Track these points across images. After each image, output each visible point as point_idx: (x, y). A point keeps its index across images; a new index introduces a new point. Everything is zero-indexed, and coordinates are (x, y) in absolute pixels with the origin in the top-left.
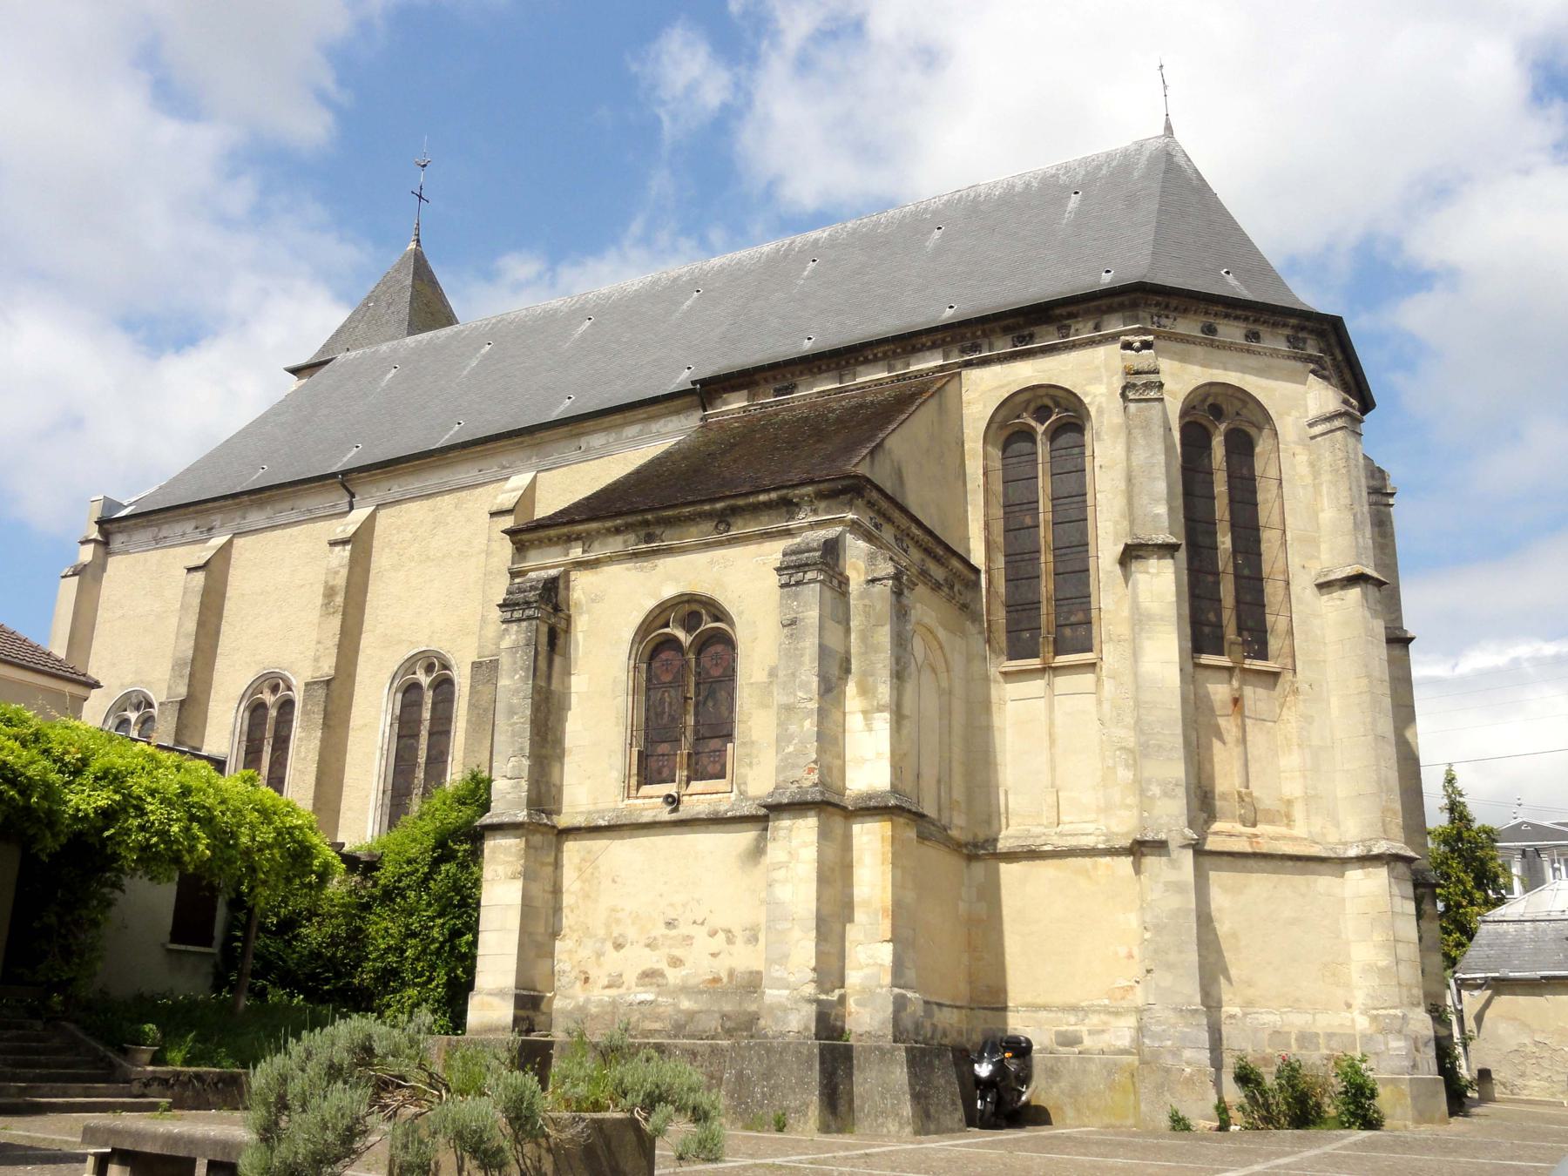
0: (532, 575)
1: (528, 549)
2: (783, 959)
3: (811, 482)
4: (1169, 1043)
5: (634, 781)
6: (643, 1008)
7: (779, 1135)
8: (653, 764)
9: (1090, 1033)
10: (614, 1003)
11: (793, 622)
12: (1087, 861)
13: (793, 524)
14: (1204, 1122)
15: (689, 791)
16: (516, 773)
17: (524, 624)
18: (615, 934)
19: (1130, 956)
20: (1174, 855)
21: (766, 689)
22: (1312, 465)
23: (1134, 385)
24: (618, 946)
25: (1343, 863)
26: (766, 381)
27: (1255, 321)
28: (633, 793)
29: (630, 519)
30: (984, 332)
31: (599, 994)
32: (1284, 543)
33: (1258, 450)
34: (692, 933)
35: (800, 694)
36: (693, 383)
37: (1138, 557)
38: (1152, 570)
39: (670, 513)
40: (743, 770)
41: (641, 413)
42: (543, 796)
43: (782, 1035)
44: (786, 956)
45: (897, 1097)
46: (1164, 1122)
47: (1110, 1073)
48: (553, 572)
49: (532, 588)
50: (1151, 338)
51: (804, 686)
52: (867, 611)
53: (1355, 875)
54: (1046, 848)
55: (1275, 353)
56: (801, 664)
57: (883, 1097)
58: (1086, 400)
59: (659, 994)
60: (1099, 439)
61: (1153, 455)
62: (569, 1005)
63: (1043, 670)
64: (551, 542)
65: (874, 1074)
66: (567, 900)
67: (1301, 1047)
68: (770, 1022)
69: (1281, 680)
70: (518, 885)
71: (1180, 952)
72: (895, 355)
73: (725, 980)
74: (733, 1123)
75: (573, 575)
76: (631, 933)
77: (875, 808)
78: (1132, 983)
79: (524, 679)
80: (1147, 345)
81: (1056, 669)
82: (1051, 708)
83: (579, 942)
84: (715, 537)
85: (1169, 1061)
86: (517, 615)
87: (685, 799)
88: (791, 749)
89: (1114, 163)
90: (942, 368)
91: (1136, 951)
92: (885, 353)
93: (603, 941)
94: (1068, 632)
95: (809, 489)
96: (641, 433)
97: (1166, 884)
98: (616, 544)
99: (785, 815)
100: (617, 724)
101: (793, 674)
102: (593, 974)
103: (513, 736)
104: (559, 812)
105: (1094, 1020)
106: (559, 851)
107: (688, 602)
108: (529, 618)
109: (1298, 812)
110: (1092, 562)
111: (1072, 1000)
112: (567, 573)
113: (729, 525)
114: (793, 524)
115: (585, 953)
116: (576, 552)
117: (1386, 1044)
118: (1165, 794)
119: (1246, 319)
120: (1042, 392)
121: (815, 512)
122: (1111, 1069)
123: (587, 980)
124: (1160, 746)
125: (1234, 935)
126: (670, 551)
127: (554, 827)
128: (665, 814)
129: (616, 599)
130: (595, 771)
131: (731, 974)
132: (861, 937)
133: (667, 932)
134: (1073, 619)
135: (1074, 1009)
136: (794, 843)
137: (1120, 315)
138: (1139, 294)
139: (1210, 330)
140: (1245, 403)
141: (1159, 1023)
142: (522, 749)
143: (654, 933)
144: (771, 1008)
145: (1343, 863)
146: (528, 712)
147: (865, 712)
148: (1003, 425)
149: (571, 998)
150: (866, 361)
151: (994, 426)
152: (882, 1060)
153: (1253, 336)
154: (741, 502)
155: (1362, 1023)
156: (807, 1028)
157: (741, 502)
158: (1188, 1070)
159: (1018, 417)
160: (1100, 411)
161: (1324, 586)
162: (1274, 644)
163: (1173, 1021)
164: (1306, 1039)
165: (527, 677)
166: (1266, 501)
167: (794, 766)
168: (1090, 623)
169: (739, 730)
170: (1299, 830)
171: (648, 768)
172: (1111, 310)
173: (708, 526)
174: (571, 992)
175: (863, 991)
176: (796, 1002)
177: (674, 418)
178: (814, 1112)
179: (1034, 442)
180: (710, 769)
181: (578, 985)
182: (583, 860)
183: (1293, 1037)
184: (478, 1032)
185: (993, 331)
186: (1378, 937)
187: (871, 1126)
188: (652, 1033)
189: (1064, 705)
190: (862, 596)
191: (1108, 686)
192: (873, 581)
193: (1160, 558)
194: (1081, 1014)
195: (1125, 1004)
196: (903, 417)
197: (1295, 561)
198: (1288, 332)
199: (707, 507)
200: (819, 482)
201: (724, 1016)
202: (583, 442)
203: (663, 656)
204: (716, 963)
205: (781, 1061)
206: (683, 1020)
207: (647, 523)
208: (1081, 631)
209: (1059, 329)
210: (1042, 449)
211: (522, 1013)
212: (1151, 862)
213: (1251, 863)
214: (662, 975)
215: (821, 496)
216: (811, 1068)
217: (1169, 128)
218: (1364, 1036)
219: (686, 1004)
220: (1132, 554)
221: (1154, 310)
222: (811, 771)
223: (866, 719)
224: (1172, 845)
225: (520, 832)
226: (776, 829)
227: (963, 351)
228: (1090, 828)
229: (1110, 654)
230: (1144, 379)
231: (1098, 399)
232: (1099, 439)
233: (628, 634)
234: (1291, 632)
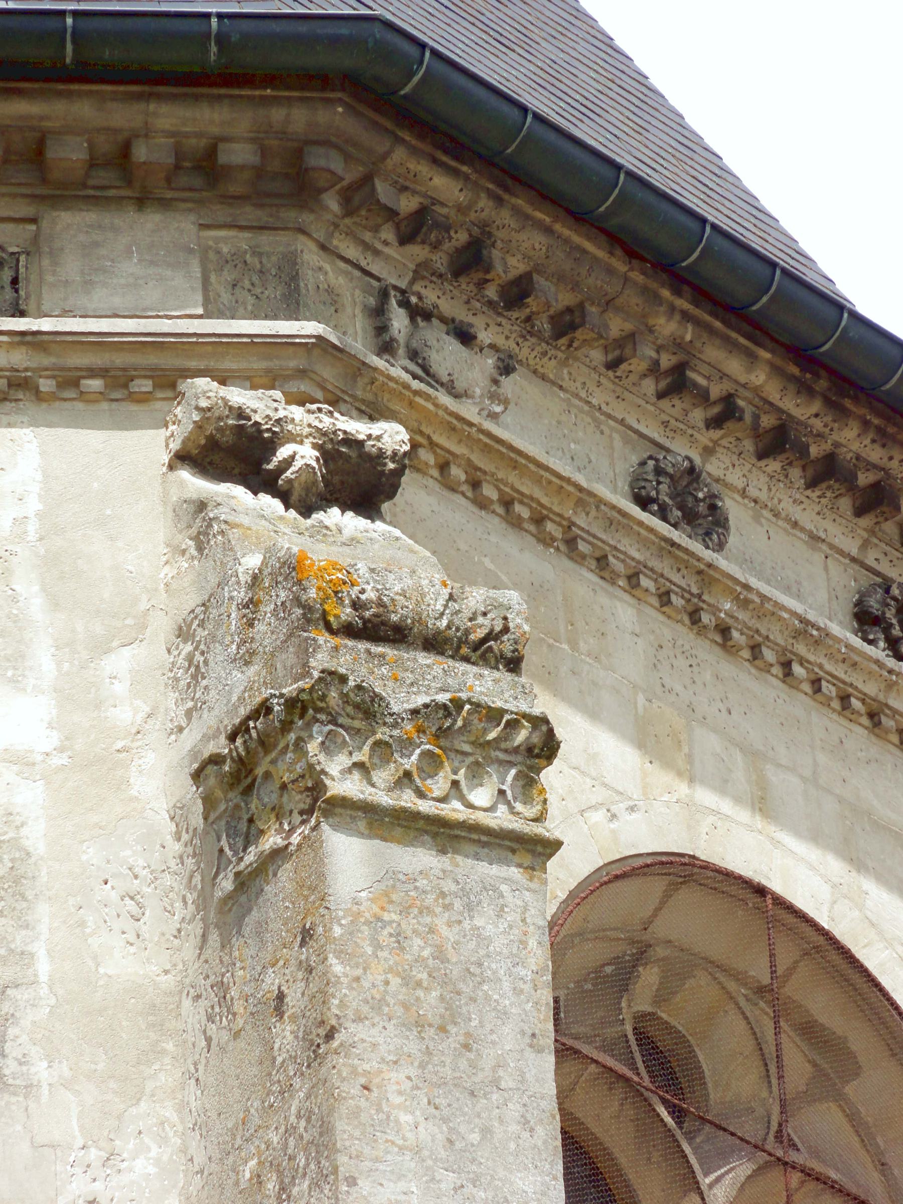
23: (368, 708)
80: (359, 483)
137: (181, 227)
138: (335, 116)
196: (389, 124)
221: (394, 263)
230: (411, 683)
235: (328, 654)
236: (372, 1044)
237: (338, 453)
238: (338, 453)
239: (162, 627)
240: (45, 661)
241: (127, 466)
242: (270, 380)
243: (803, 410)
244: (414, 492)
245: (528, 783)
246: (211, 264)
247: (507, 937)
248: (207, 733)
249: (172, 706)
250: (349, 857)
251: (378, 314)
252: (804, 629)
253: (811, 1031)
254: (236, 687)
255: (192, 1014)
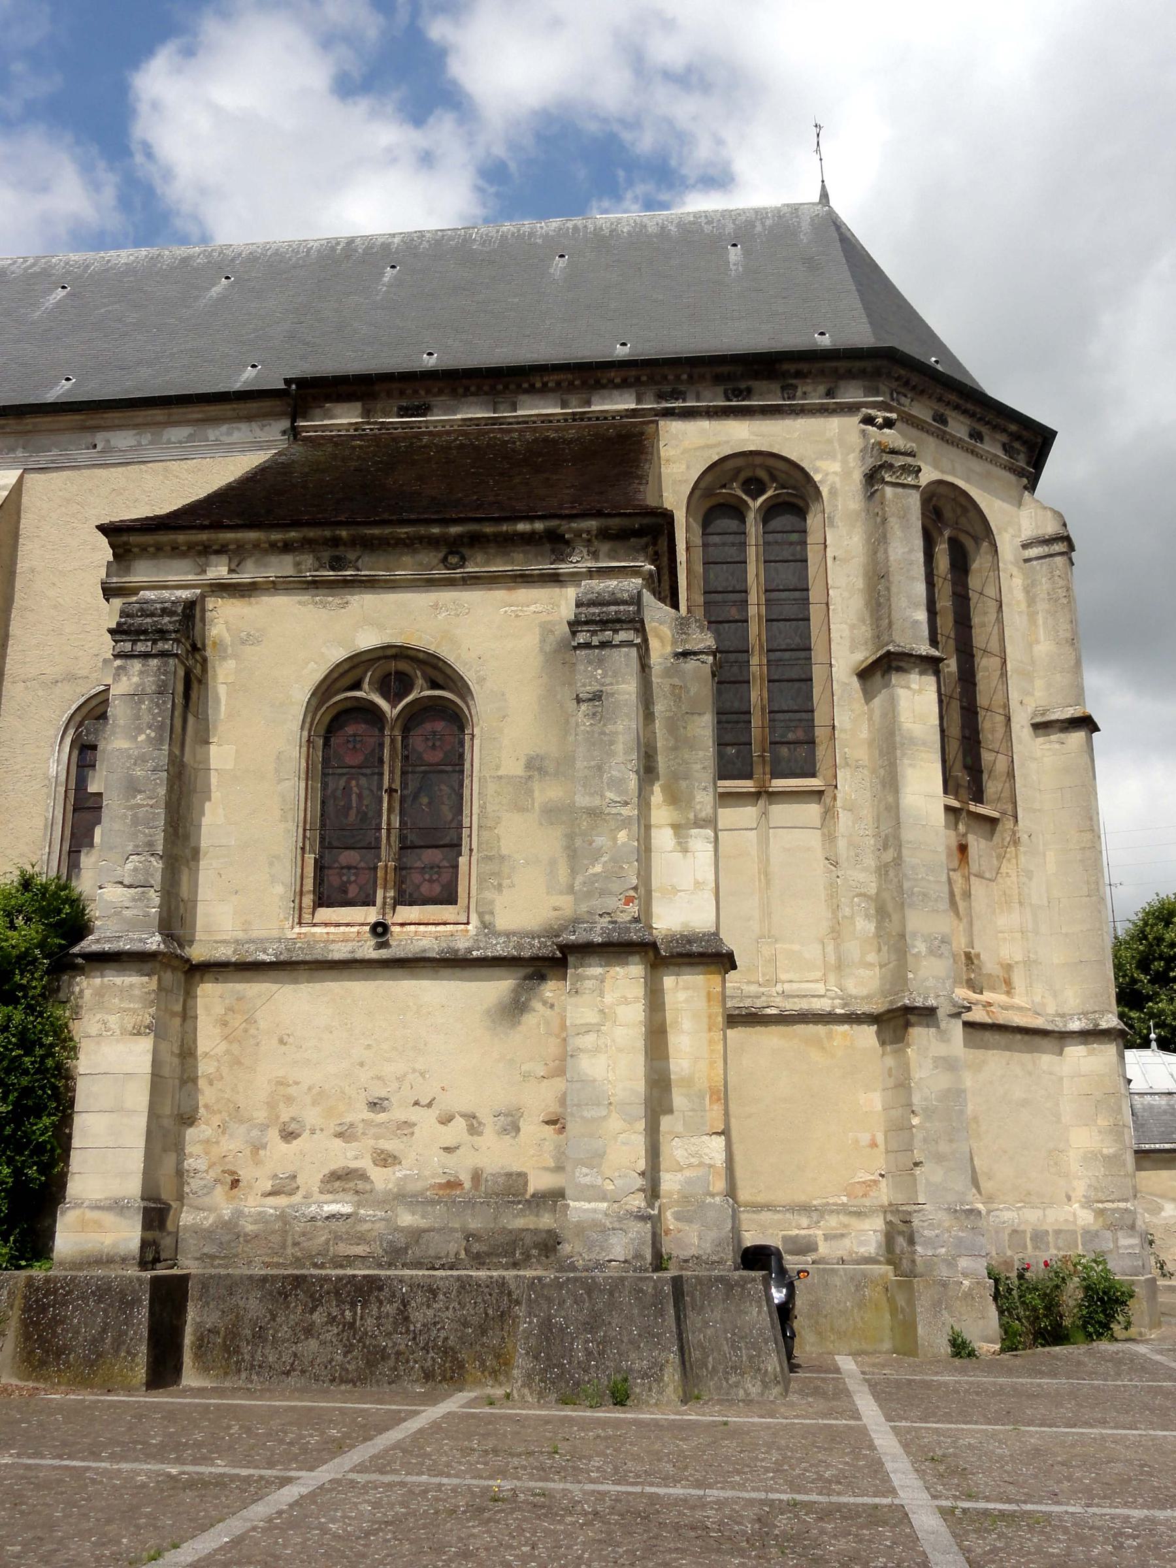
0: (150, 595)
1: (137, 557)
2: (595, 1159)
3: (599, 514)
4: (943, 1250)
5: (308, 900)
6: (334, 1225)
7: (618, 1414)
8: (333, 878)
9: (827, 1237)
10: (283, 1217)
11: (597, 697)
12: (820, 1029)
13: (564, 568)
14: (987, 1347)
15: (398, 918)
16: (141, 878)
17: (154, 662)
18: (285, 1117)
19: (874, 1145)
20: (943, 1025)
21: (523, 786)
22: (1027, 590)
23: (891, 466)
24: (289, 1135)
25: (1063, 1037)
26: (389, 395)
27: (980, 420)
28: (307, 917)
29: (312, 533)
30: (691, 377)
31: (256, 1205)
32: (1004, 674)
33: (975, 566)
34: (413, 1119)
35: (610, 795)
36: (288, 382)
37: (899, 669)
38: (915, 686)
39: (376, 531)
40: (488, 895)
41: (195, 412)
42: (175, 919)
43: (599, 1266)
44: (600, 1155)
45: (754, 1346)
46: (946, 1349)
47: (858, 1287)
48: (185, 594)
49: (165, 612)
50: (894, 416)
51: (617, 784)
52: (677, 693)
53: (1075, 1052)
54: (769, 1011)
55: (993, 460)
56: (611, 754)
57: (734, 1347)
58: (817, 478)
59: (359, 1205)
60: (832, 525)
61: (911, 551)
62: (207, 1220)
63: (757, 795)
64: (176, 552)
65: (717, 1315)
66: (205, 1067)
67: (1036, 1248)
68: (578, 1248)
69: (1000, 827)
70: (144, 1047)
71: (951, 1141)
72: (571, 388)
73: (467, 1185)
74: (541, 1395)
75: (210, 603)
76: (312, 1116)
77: (701, 955)
78: (876, 1177)
79: (157, 742)
80: (888, 424)
81: (773, 793)
82: (764, 842)
83: (223, 1128)
84: (440, 572)
85: (944, 1272)
86: (141, 647)
87: (395, 929)
88: (598, 868)
89: (768, 222)
90: (634, 413)
91: (880, 1139)
92: (558, 384)
93: (264, 1128)
94: (784, 751)
95: (592, 524)
96: (191, 438)
97: (936, 1059)
98: (282, 567)
99: (594, 960)
100: (284, 819)
101: (599, 768)
102: (244, 1174)
103: (135, 821)
104: (191, 942)
105: (832, 1221)
106: (189, 995)
107: (395, 657)
108: (163, 654)
109: (1018, 979)
110: (817, 672)
111: (801, 1198)
112: (203, 597)
113: (463, 559)
114: (564, 568)
115: (232, 1144)
116: (219, 571)
117: (1116, 1241)
118: (931, 952)
119: (972, 415)
120: (758, 460)
121: (595, 555)
122: (859, 1283)
123: (235, 1183)
124: (925, 895)
125: (975, 1119)
126: (371, 584)
127: (188, 961)
128: (368, 950)
129: (281, 646)
130: (249, 882)
131: (476, 1176)
132: (679, 1128)
133: (371, 1116)
134: (791, 736)
135: (805, 1209)
136: (608, 999)
137: (860, 383)
139: (941, 419)
140: (965, 510)
141: (932, 1226)
142: (150, 844)
143: (348, 1119)
144: (581, 1229)
145: (1063, 1037)
146: (162, 791)
147: (676, 827)
148: (709, 493)
149: (210, 1209)
150: (531, 390)
151: (698, 493)
152: (728, 1295)
153: (976, 436)
154: (488, 529)
155: (1086, 1218)
156: (638, 1256)
157: (488, 529)
158: (966, 1283)
159: (724, 486)
160: (833, 492)
161: (1042, 727)
162: (991, 788)
163: (947, 1224)
164: (1039, 1237)
165: (160, 740)
166: (983, 625)
167: (603, 893)
168: (812, 742)
169: (473, 838)
170: (1018, 1000)
171: (329, 888)
172: (850, 375)
173: (430, 557)
174: (207, 1200)
175: (685, 1199)
176: (620, 1219)
177: (244, 426)
178: (671, 1376)
179: (742, 519)
180: (425, 889)
181: (219, 1192)
182: (230, 1009)
183: (1029, 1235)
184: (78, 1265)
185: (702, 378)
186: (1103, 1122)
187: (719, 1388)
188: (350, 1260)
189: (780, 841)
190: (668, 672)
191: (844, 820)
192: (685, 654)
193: (922, 673)
194: (815, 1216)
195: (867, 1202)
197: (1014, 696)
198: (1004, 438)
199: (436, 530)
200: (609, 515)
201: (469, 1236)
202: (100, 438)
203: (350, 730)
204: (451, 1160)
205: (612, 1306)
206: (402, 1241)
207: (336, 542)
208: (802, 751)
209: (783, 388)
210: (753, 527)
211: (150, 1235)
212: (919, 1034)
213: (988, 1036)
214: (363, 1176)
215: (604, 535)
216: (661, 1313)
217: (824, 195)
218: (1086, 1232)
219: (407, 1219)
220: (883, 667)
221: (894, 385)
222: (629, 900)
223: (677, 835)
224: (941, 1013)
225: (147, 967)
226: (581, 978)
227: (661, 397)
228: (820, 988)
229: (852, 785)
230: (899, 461)
231: (831, 478)
232: (832, 525)
233: (301, 694)
234: (1011, 775)
235: (886, 458)
236: (893, 521)
237: (886, 420)
238: (886, 420)
239: (858, 450)
240: (839, 456)
241: (852, 422)
242: (874, 408)
243: (961, 402)
244: (898, 424)
245: (917, 477)
246: (865, 387)
247: (914, 501)
248: (866, 468)
249: (860, 463)
250: (889, 491)
251: (892, 394)
252: (960, 439)
253: (962, 506)
254: (870, 462)
255: (863, 514)
